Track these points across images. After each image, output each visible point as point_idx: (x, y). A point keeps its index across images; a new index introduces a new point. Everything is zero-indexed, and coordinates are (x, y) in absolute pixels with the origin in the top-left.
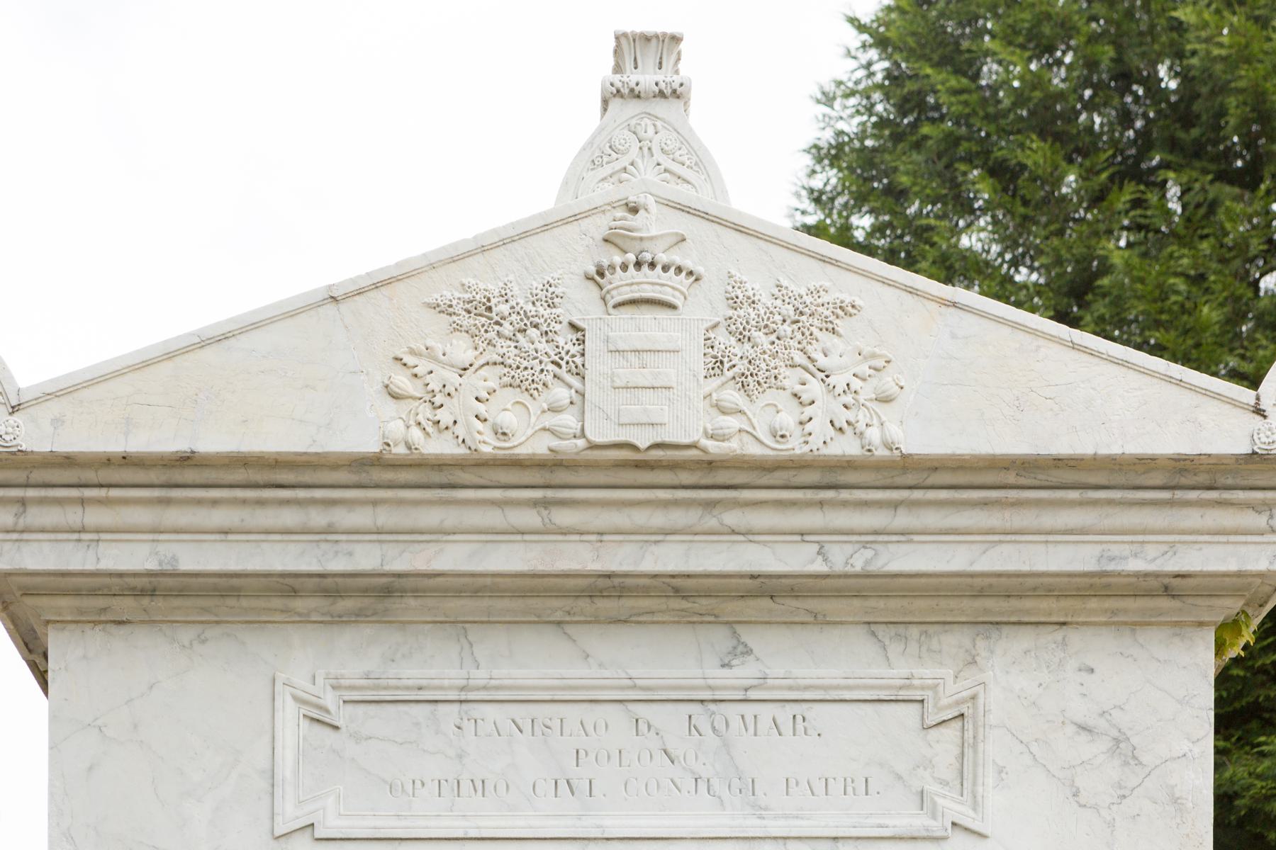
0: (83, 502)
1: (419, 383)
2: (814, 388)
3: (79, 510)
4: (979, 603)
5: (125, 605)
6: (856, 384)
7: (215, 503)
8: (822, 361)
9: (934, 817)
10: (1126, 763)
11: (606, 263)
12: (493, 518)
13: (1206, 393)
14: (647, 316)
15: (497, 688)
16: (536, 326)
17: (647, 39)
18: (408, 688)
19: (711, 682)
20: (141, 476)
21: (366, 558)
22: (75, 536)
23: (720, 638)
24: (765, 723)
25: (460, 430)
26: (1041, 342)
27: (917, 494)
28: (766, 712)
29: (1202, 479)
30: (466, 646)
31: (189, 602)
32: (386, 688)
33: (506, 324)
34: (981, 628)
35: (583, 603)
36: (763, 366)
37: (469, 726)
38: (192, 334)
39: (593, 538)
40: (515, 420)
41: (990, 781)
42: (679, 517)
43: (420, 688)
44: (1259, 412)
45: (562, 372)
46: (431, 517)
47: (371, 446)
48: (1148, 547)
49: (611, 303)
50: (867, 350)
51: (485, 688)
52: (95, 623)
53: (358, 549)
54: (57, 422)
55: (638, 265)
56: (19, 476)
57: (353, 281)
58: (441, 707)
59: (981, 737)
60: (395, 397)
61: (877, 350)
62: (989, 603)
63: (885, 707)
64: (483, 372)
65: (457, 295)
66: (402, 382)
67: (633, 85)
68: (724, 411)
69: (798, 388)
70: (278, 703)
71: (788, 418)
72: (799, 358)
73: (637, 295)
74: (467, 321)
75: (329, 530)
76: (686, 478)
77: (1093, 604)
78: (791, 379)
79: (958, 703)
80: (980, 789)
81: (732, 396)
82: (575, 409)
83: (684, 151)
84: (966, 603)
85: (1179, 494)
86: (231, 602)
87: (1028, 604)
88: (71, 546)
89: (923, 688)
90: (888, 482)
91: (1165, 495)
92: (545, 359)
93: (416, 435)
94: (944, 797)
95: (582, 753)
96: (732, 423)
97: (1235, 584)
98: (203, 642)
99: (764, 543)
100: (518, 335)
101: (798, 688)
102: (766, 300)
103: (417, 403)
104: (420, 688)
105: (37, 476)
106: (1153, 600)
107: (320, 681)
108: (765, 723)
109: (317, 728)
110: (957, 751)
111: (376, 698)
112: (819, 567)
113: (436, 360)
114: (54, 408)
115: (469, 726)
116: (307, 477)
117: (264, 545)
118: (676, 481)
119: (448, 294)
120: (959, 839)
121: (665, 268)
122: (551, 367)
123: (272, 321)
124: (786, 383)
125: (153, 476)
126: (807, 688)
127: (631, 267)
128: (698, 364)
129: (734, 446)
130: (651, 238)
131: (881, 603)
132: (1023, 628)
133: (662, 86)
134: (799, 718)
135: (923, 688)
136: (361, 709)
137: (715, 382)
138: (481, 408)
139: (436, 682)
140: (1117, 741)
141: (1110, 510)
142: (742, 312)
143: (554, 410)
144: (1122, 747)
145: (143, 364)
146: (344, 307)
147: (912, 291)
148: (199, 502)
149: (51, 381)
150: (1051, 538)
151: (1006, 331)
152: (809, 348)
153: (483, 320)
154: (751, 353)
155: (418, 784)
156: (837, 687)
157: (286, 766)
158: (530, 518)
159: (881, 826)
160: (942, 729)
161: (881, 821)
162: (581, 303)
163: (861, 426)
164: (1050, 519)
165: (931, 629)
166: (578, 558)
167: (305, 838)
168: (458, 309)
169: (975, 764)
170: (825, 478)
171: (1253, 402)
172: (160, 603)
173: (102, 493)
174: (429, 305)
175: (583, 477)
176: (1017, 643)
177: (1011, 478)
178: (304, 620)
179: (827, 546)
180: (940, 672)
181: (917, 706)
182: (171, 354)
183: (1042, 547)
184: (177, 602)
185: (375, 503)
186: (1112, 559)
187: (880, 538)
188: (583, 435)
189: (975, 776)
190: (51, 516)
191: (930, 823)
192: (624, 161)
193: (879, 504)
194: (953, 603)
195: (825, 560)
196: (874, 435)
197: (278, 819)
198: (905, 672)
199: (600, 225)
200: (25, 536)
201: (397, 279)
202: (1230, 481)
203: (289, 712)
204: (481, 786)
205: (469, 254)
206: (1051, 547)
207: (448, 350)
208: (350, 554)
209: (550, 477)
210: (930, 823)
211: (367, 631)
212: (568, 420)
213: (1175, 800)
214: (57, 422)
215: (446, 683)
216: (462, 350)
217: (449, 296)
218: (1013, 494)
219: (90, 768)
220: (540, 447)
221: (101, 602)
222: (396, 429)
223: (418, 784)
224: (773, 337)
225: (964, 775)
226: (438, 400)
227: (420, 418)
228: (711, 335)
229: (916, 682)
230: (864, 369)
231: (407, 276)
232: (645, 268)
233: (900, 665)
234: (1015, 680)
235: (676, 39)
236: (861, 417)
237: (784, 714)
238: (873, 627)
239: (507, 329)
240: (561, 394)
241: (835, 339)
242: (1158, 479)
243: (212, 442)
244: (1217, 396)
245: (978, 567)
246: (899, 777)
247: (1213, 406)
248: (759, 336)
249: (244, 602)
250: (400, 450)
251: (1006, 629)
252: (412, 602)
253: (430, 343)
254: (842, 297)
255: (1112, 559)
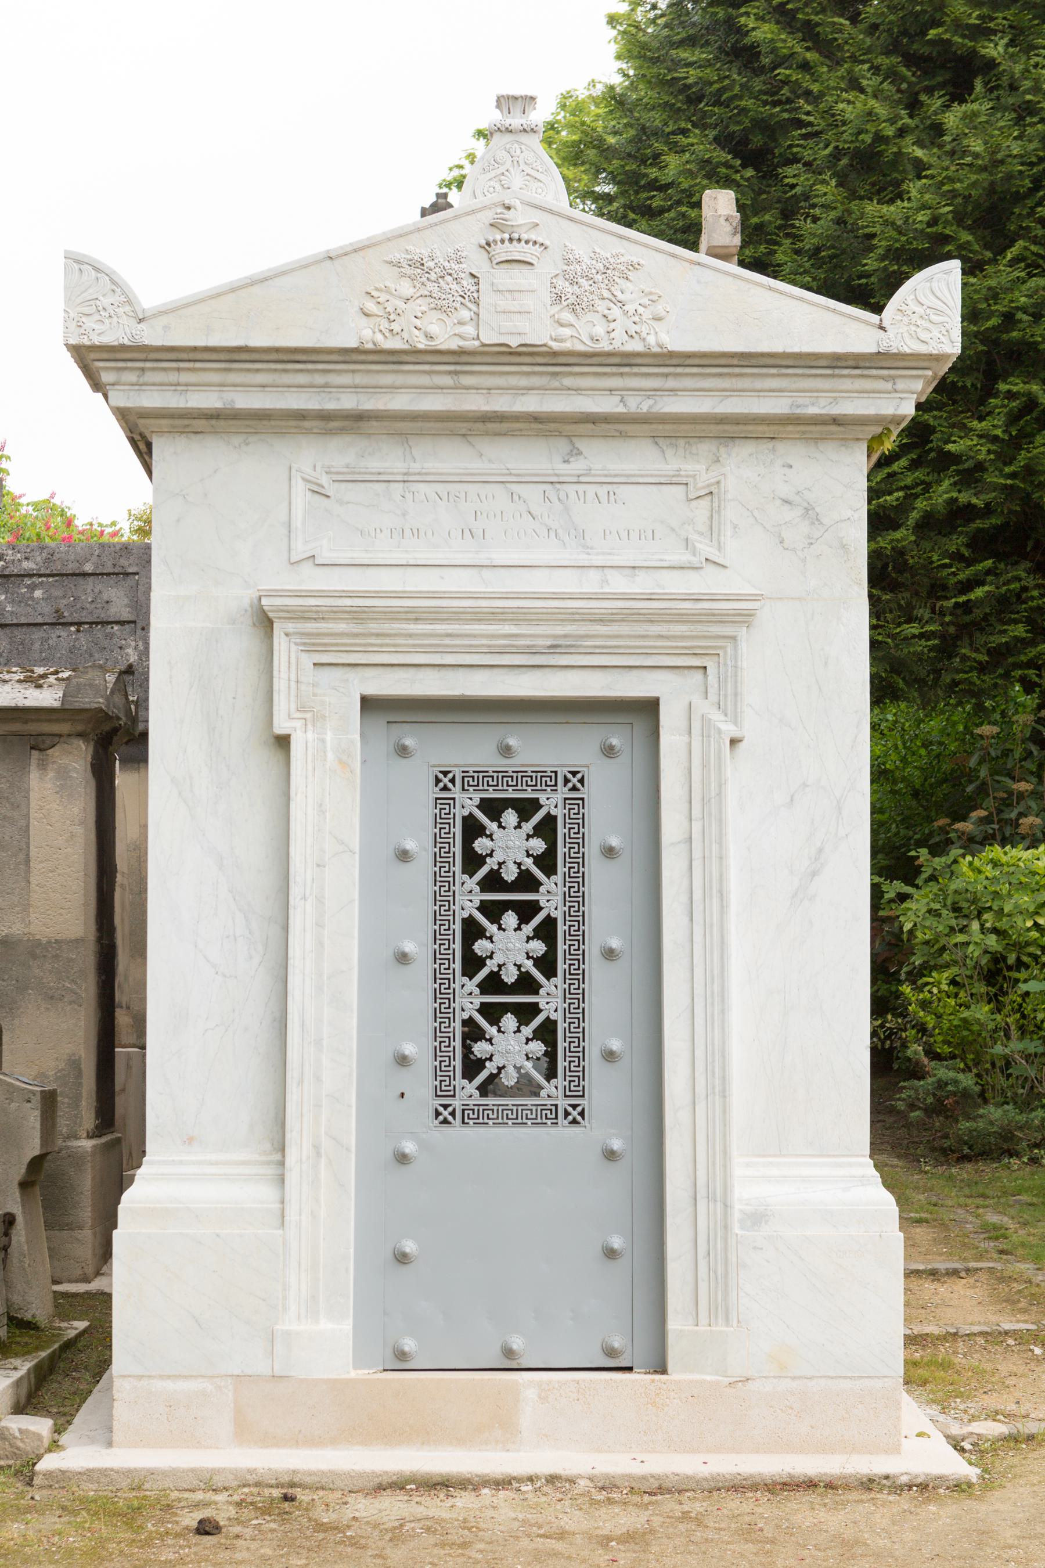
0: (178, 369)
1: (380, 307)
2: (616, 312)
3: (176, 373)
4: (720, 427)
5: (201, 424)
6: (641, 310)
7: (258, 370)
8: (620, 296)
9: (695, 555)
10: (813, 523)
11: (491, 239)
12: (425, 380)
13: (850, 316)
14: (516, 271)
15: (426, 474)
16: (450, 275)
17: (516, 98)
18: (372, 474)
19: (557, 472)
20: (214, 356)
21: (348, 402)
22: (173, 388)
23: (563, 445)
24: (591, 495)
25: (405, 335)
26: (751, 286)
27: (679, 370)
28: (591, 490)
29: (850, 363)
30: (408, 448)
31: (239, 423)
32: (359, 473)
33: (432, 273)
34: (722, 440)
35: (479, 425)
36: (585, 299)
37: (409, 496)
38: (246, 278)
39: (485, 391)
40: (437, 329)
41: (729, 534)
42: (536, 381)
43: (379, 474)
44: (882, 328)
45: (466, 302)
46: (388, 379)
47: (353, 344)
48: (820, 400)
49: (495, 262)
50: (647, 290)
51: (419, 474)
52: (182, 433)
53: (343, 396)
54: (166, 328)
55: (511, 240)
56: (142, 356)
57: (341, 248)
58: (392, 485)
59: (722, 507)
60: (367, 315)
61: (653, 290)
62: (727, 427)
63: (664, 487)
64: (418, 301)
65: (403, 256)
66: (371, 306)
67: (507, 126)
68: (562, 325)
69: (606, 312)
70: (293, 482)
71: (600, 330)
72: (606, 294)
73: (510, 258)
74: (409, 271)
75: (326, 386)
76: (539, 360)
77: (790, 428)
78: (601, 306)
79: (708, 486)
80: (722, 538)
81: (567, 316)
82: (473, 323)
83: (538, 163)
84: (712, 427)
85: (837, 371)
86: (265, 422)
87: (751, 428)
88: (170, 393)
89: (687, 476)
90: (661, 363)
91: (829, 372)
92: (456, 294)
93: (379, 337)
94: (701, 542)
95: (478, 513)
96: (567, 332)
97: (876, 420)
98: (247, 444)
99: (588, 395)
100: (440, 280)
101: (610, 476)
102: (586, 260)
103: (379, 319)
104: (379, 474)
105: (152, 356)
106: (832, 427)
107: (318, 468)
108: (591, 495)
109: (317, 496)
110: (708, 514)
111: (353, 479)
112: (621, 409)
113: (391, 294)
114: (164, 320)
115: (409, 496)
116: (314, 358)
117: (286, 394)
118: (534, 362)
119: (398, 256)
120: (710, 569)
121: (527, 242)
122: (460, 299)
123: (293, 270)
124: (599, 309)
125: (222, 356)
126: (616, 476)
127: (507, 242)
128: (547, 298)
129: (567, 346)
130: (518, 226)
131: (661, 427)
132: (748, 441)
133: (525, 126)
134: (611, 493)
135: (687, 476)
136: (343, 485)
137: (557, 308)
138: (418, 322)
139: (390, 470)
140: (807, 510)
141: (796, 379)
142: (572, 268)
143: (461, 323)
144: (809, 512)
145: (217, 295)
146: (336, 262)
147: (674, 256)
148: (249, 370)
149: (163, 304)
150: (761, 394)
151: (730, 279)
152: (612, 289)
153: (419, 271)
154: (578, 291)
155: (378, 531)
156: (634, 476)
157: (297, 522)
158: (447, 381)
159: (661, 560)
160: (699, 501)
161: (662, 557)
162: (478, 262)
163: (644, 335)
164: (759, 384)
165: (692, 441)
166: (475, 403)
167: (310, 563)
168: (404, 264)
169: (719, 523)
170: (624, 361)
171: (878, 322)
172: (222, 423)
173: (191, 365)
174: (387, 262)
175: (478, 359)
176: (746, 449)
177: (735, 362)
178: (309, 432)
179: (626, 398)
180: (698, 467)
181: (683, 487)
182: (234, 289)
183: (756, 399)
184: (232, 422)
185: (353, 371)
186: (798, 406)
187: (658, 393)
188: (478, 338)
189: (719, 530)
190: (159, 377)
191: (692, 558)
192: (502, 169)
193: (657, 375)
194: (704, 427)
195: (625, 405)
196: (651, 340)
197: (293, 553)
198: (676, 467)
199: (488, 216)
200: (143, 388)
201: (368, 247)
202: (868, 365)
203: (300, 488)
204: (417, 533)
205: (411, 233)
206: (762, 399)
207: (398, 287)
208: (338, 399)
209: (459, 359)
210: (692, 558)
211: (348, 439)
212: (469, 330)
213: (843, 546)
214: (166, 328)
215: (395, 471)
216: (406, 288)
217: (398, 256)
218: (737, 370)
219: (178, 521)
220: (454, 345)
221: (186, 422)
222: (367, 334)
223: (378, 531)
224: (591, 282)
225: (713, 530)
226: (392, 317)
227: (382, 328)
228: (554, 281)
229: (683, 473)
230: (645, 301)
231: (374, 245)
232: (515, 242)
233: (673, 462)
234: (745, 473)
235: (532, 99)
236: (643, 329)
237: (602, 491)
238: (656, 439)
239: (433, 276)
240: (465, 314)
241: (629, 284)
242: (824, 363)
243: (258, 340)
244: (856, 319)
245: (717, 410)
246: (673, 530)
247: (856, 325)
248: (582, 281)
249: (273, 423)
250: (369, 346)
251: (737, 441)
252: (375, 423)
253: (388, 284)
254: (632, 259)
255: (798, 406)
